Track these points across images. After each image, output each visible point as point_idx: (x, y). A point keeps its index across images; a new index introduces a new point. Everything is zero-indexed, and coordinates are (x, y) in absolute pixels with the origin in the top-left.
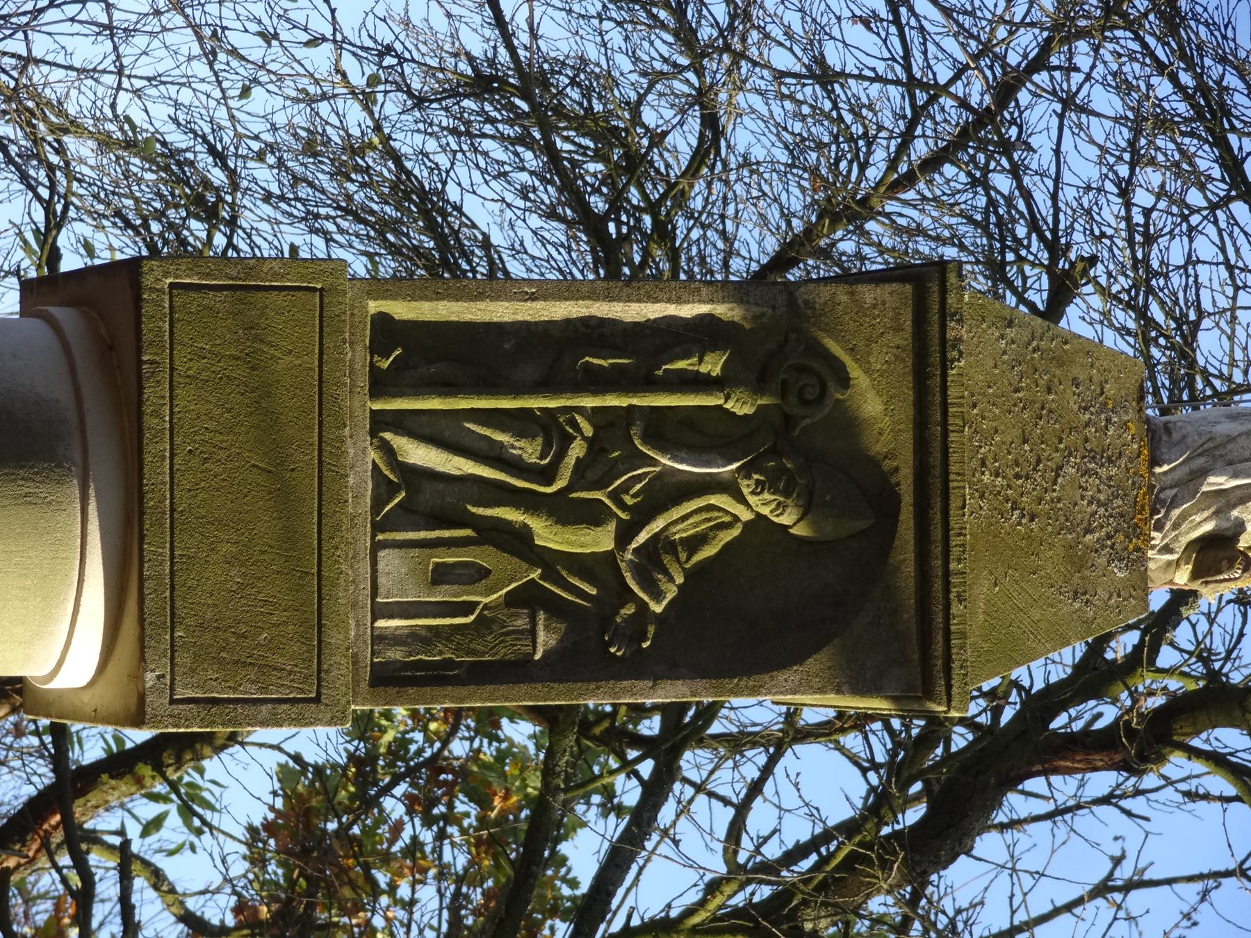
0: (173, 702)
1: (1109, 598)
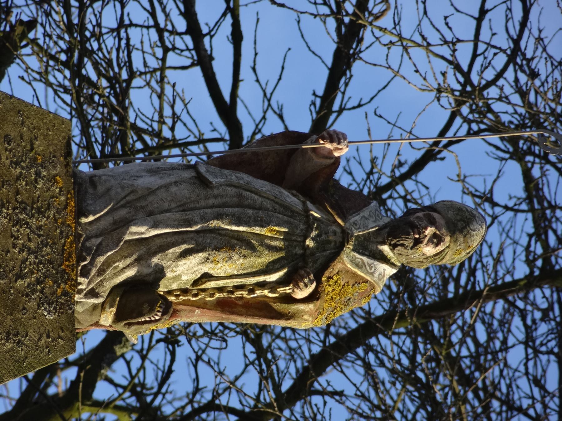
1: (40, 339)
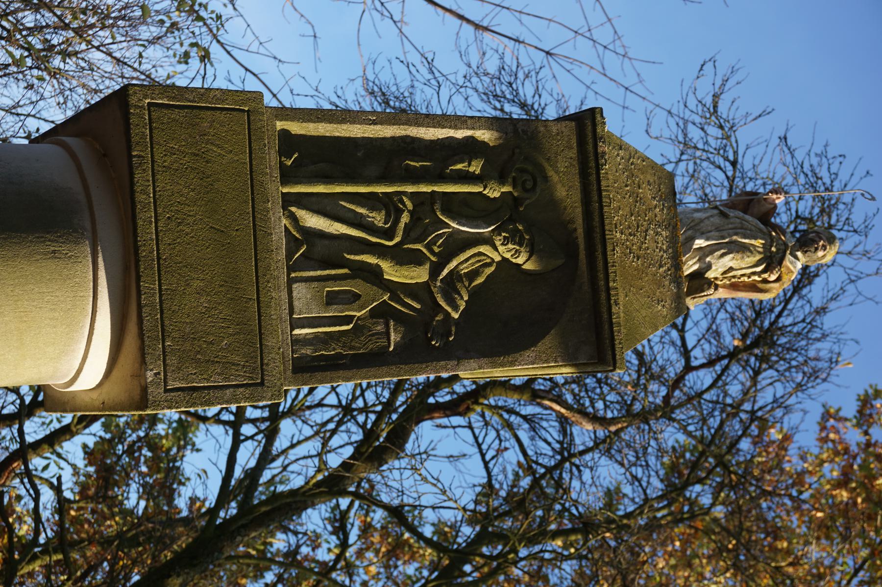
0: (166, 391)
